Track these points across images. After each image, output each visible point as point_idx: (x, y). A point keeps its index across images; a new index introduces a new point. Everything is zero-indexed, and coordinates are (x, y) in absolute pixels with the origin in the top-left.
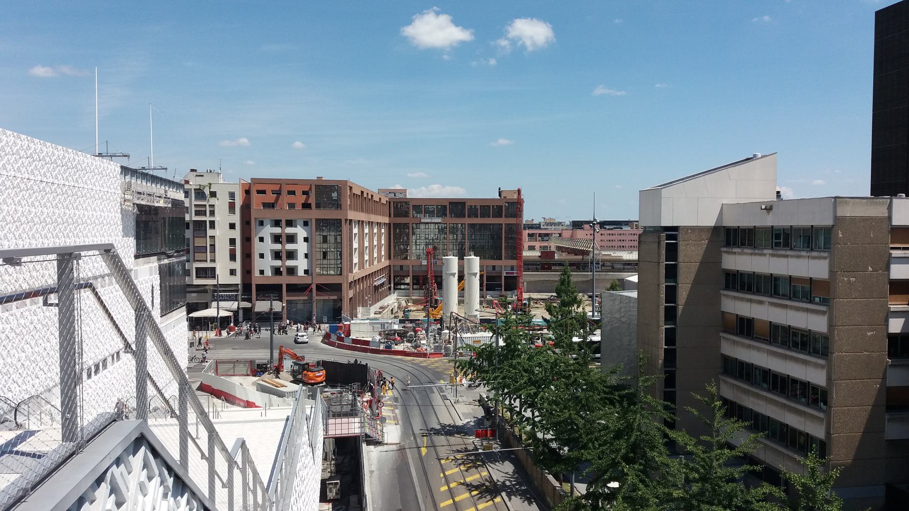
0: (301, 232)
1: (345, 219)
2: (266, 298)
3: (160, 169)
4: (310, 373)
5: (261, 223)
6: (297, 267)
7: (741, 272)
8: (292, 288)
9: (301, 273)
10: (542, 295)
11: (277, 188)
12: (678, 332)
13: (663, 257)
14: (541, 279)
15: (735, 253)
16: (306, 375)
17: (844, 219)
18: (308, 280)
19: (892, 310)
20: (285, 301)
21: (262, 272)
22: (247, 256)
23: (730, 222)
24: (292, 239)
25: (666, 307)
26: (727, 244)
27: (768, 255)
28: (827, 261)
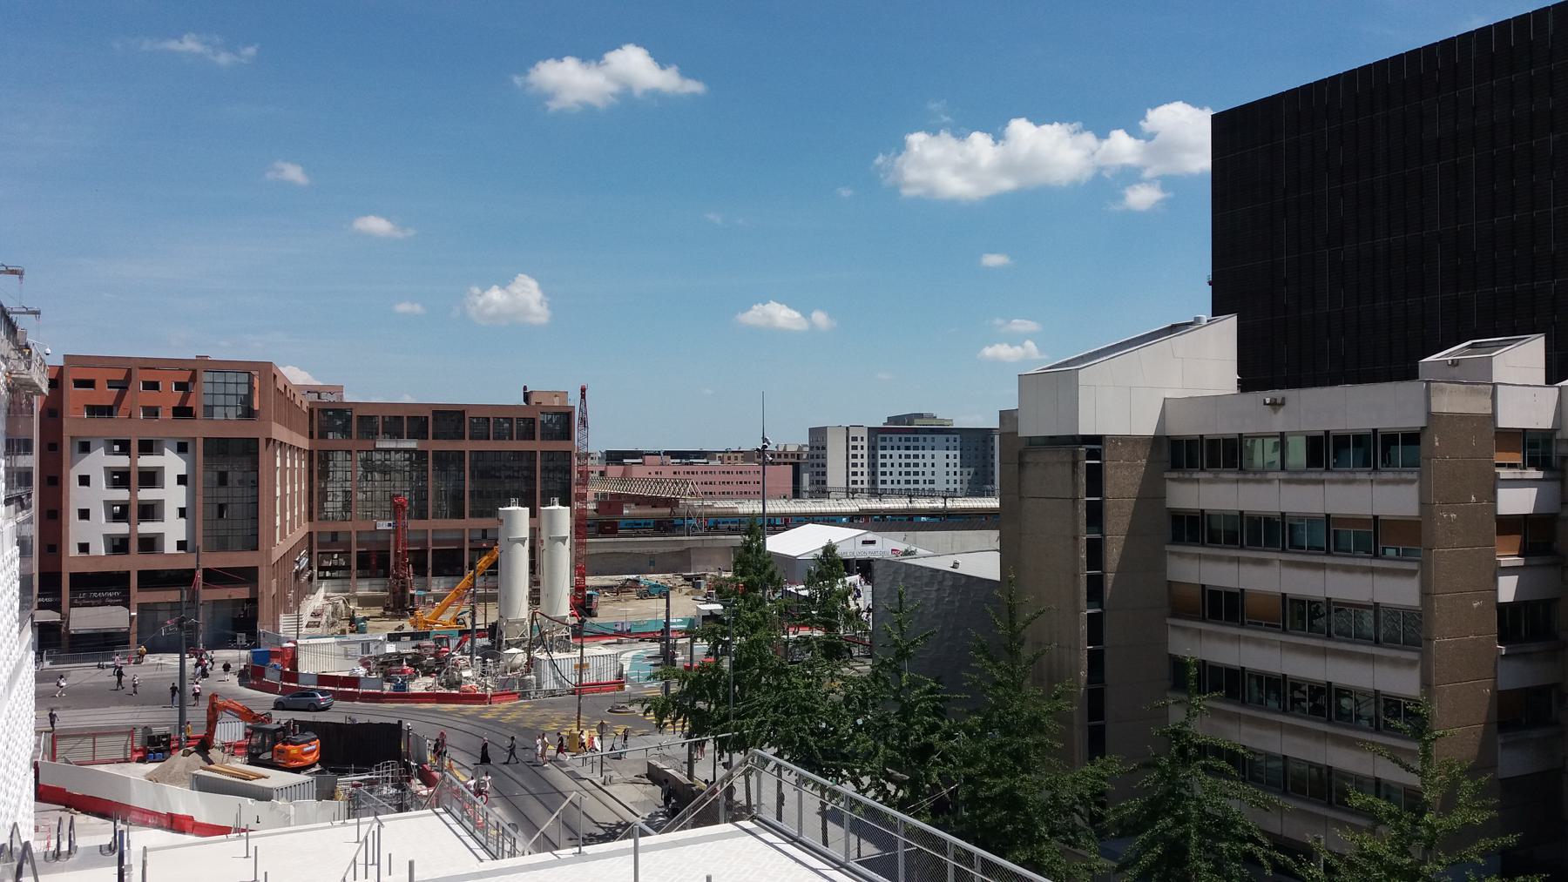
0: (172, 464)
1: (267, 439)
2: (93, 602)
3: (23, 313)
4: (290, 747)
5: (85, 448)
6: (161, 535)
7: (1209, 512)
8: (150, 579)
9: (170, 547)
10: (603, 579)
11: (120, 375)
12: (1107, 619)
13: (1083, 489)
14: (603, 550)
15: (1198, 480)
16: (281, 751)
17: (1440, 416)
18: (188, 562)
19: (1502, 565)
20: (134, 606)
21: (84, 548)
22: (52, 516)
23: (1183, 428)
24: (151, 478)
25: (1088, 576)
26: (1172, 467)
27: (1277, 482)
28: (1416, 486)
